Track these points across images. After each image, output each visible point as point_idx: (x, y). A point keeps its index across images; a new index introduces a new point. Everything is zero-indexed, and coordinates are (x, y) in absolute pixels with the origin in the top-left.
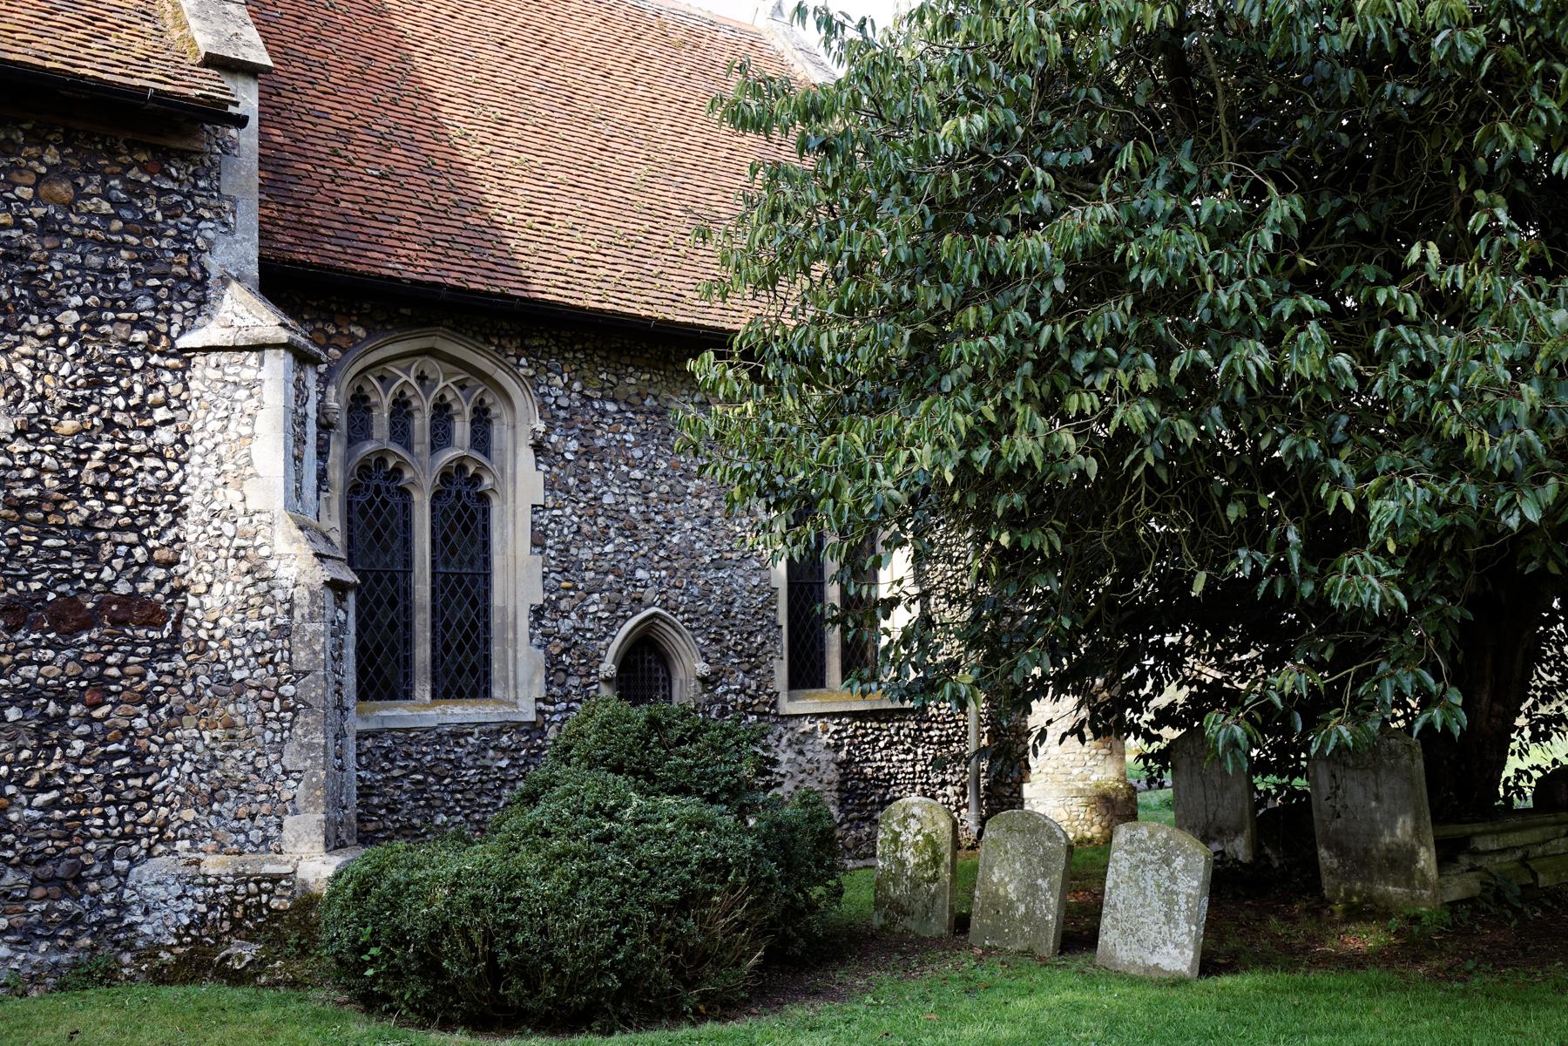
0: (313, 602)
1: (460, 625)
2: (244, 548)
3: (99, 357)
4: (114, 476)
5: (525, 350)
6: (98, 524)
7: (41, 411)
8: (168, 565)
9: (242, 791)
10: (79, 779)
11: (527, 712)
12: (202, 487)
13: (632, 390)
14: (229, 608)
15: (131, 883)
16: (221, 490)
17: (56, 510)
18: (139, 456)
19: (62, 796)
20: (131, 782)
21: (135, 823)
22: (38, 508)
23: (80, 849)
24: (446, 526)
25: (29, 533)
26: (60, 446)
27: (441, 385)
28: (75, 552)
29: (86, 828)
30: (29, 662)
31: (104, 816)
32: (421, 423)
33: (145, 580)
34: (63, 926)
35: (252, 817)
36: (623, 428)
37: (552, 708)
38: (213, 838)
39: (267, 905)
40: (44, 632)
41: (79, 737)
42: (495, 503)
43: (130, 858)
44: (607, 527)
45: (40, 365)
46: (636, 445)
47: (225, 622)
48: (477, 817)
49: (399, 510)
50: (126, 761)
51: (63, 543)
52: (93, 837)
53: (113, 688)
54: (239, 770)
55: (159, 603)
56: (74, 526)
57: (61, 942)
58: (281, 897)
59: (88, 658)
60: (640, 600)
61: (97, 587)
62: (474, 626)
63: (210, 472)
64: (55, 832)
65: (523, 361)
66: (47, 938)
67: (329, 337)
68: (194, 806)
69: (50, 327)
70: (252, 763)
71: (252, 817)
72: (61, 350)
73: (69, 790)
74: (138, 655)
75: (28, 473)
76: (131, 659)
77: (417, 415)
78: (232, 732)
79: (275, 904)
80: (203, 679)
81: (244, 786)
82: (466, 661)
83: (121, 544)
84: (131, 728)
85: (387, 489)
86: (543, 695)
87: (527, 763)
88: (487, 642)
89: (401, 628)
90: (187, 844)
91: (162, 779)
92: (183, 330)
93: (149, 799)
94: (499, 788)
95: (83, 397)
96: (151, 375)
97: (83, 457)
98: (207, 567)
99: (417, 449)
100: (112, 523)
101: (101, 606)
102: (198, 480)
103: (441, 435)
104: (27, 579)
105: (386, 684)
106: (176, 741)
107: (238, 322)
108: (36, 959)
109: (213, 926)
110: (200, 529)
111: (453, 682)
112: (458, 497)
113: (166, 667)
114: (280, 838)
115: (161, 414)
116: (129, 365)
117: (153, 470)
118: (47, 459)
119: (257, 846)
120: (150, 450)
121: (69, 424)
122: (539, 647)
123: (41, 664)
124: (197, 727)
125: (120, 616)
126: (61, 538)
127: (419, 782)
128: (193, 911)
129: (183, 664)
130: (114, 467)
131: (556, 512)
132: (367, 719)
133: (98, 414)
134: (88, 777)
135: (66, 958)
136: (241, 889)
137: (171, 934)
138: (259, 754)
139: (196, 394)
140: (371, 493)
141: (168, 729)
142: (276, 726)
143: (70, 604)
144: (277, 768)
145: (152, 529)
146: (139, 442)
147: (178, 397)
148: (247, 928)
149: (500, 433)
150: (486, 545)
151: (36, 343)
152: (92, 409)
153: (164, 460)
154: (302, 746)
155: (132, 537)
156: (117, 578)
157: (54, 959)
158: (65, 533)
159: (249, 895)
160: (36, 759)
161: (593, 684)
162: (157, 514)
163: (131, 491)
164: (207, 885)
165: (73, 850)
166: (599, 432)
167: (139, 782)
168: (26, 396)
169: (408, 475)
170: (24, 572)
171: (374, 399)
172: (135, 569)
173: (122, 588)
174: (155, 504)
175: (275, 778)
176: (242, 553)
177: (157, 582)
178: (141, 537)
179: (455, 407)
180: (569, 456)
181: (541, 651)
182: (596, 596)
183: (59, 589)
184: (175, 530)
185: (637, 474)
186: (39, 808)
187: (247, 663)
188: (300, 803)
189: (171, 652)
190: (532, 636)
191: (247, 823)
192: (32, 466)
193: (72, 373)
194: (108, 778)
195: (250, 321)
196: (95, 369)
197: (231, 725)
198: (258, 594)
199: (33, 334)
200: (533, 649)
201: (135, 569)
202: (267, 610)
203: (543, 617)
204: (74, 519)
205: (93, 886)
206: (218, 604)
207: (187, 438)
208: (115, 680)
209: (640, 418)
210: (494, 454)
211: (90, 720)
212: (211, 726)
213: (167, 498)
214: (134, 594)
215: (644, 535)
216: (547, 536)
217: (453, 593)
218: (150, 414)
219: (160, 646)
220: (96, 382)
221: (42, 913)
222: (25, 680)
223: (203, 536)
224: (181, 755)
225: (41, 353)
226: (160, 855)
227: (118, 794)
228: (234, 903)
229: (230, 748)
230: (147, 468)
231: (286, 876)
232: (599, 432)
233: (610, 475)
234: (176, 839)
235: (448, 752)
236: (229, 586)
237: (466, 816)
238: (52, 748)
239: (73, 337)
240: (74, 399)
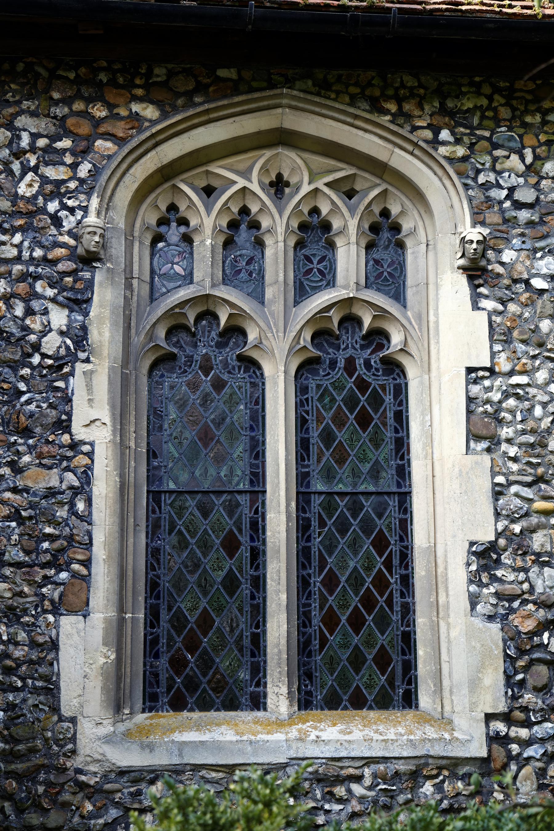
1: (356, 580)
5: (454, 118)
11: (472, 742)
24: (328, 416)
27: (306, 189)
37: (524, 733)
62: (381, 583)
65: (445, 135)
67: (97, 122)
82: (369, 643)
86: (502, 707)
88: (408, 611)
89: (245, 589)
105: (219, 686)
122: (491, 618)
131: (516, 379)
132: (151, 748)
150: (402, 446)
180: (538, 283)
200: (478, 623)
216: (500, 422)
217: (343, 527)
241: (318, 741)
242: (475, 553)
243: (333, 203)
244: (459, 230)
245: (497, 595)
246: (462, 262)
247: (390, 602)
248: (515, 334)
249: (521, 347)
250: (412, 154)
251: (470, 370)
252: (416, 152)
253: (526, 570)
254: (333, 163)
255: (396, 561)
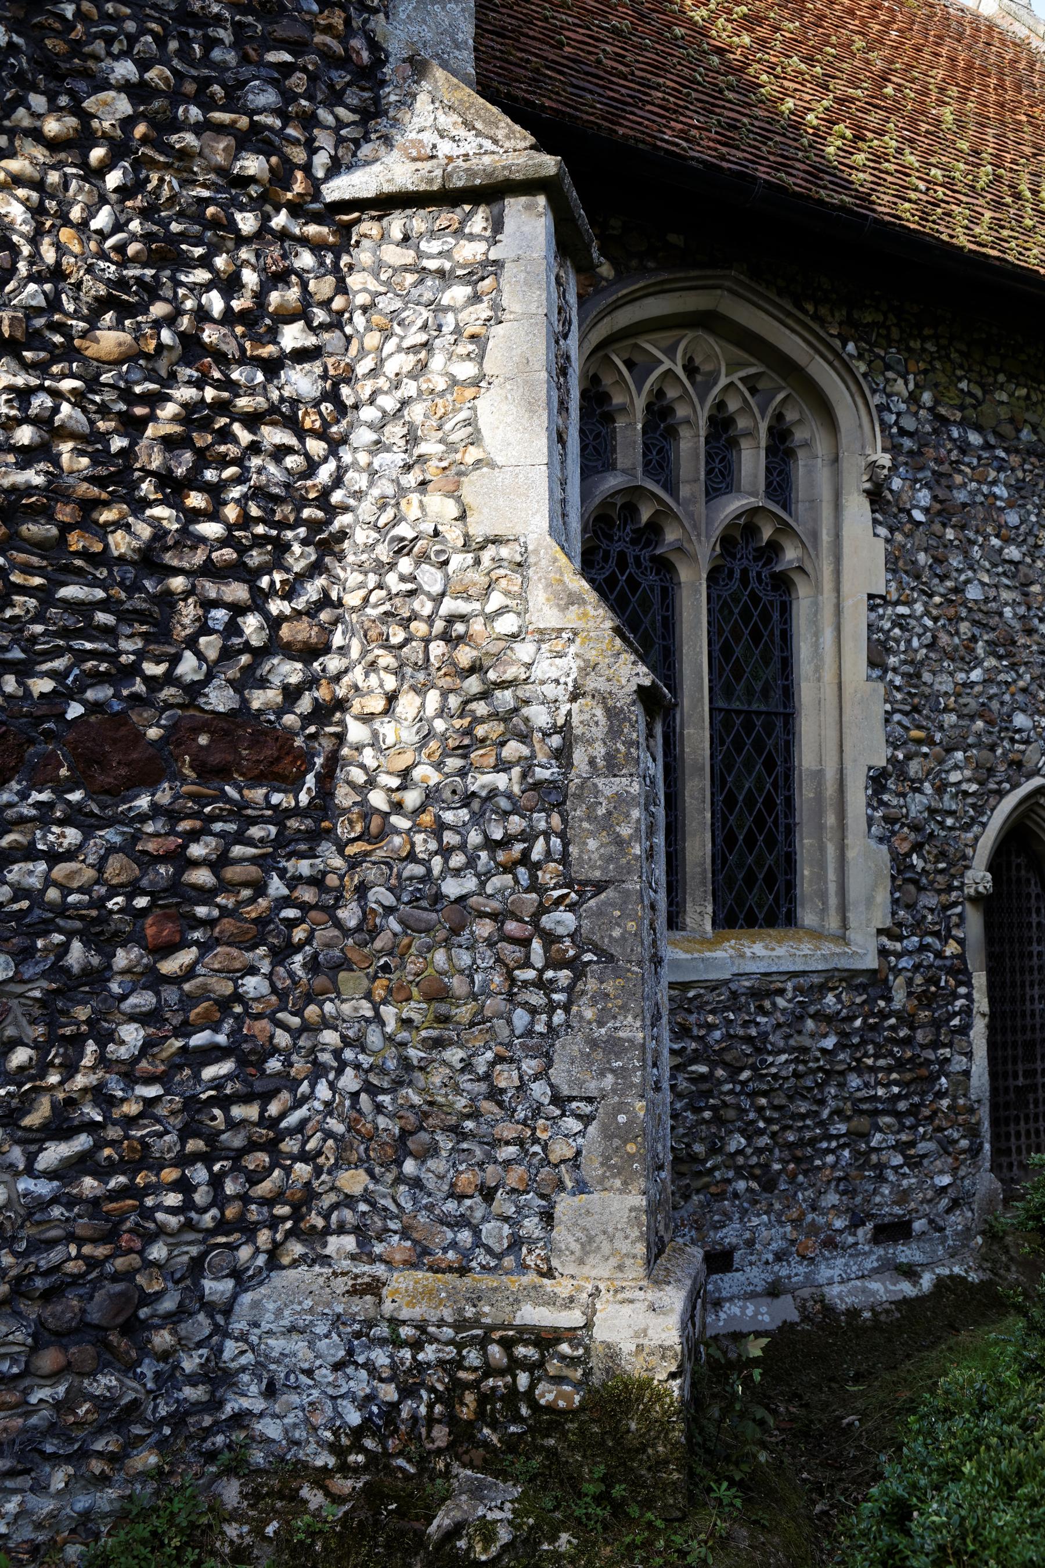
0: (613, 733)
2: (463, 618)
3: (173, 199)
4: (203, 460)
5: (853, 329)
6: (170, 559)
7: (54, 304)
8: (310, 653)
9: (463, 1136)
10: (132, 1109)
12: (376, 492)
13: (1003, 413)
14: (433, 745)
15: (238, 1326)
16: (415, 497)
17: (86, 522)
18: (253, 421)
19: (98, 1146)
20: (237, 1112)
21: (245, 1199)
22: (45, 513)
23: (135, 1260)
25: (28, 570)
26: (93, 384)
27: (723, 381)
28: (125, 616)
29: (147, 1214)
30: (29, 853)
31: (184, 1186)
32: (690, 446)
33: (263, 683)
34: (100, 1430)
35: (488, 1194)
36: (993, 474)
37: (898, 946)
38: (405, 1233)
39: (529, 1395)
40: (61, 788)
41: (132, 1018)
42: (803, 590)
43: (237, 1274)
44: (974, 639)
45: (51, 205)
46: (1011, 505)
47: (426, 773)
48: (791, 1137)
49: (656, 598)
50: (226, 1067)
51: (100, 594)
52: (162, 1230)
53: (201, 911)
54: (458, 1091)
55: (291, 733)
56: (121, 558)
57: (97, 1466)
58: (558, 1380)
59: (151, 846)
60: (1019, 764)
61: (168, 693)
62: (770, 803)
63: (391, 460)
64: (83, 1226)
66: (68, 1459)
68: (363, 1162)
69: (72, 121)
70: (487, 1077)
71: (488, 1194)
72: (95, 174)
73: (113, 1133)
74: (250, 842)
75: (25, 435)
76: (238, 850)
77: (684, 432)
78: (443, 1008)
79: (546, 1394)
80: (380, 895)
81: (469, 1125)
82: (760, 861)
83: (216, 604)
84: (237, 997)
85: (637, 558)
86: (888, 923)
87: (864, 1042)
88: (790, 831)
90: (349, 1242)
91: (298, 1104)
92: (335, 168)
93: (271, 1147)
94: (820, 1086)
95: (139, 280)
96: (275, 251)
97: (139, 411)
98: (387, 659)
99: (685, 491)
100: (199, 558)
101: (177, 735)
102: (367, 474)
103: (721, 478)
104: (24, 671)
106: (326, 1023)
107: (445, 148)
108: (46, 1506)
109: (413, 1435)
110: (372, 580)
111: (740, 901)
112: (745, 580)
113: (304, 867)
114: (548, 1243)
115: (293, 336)
116: (232, 226)
117: (280, 453)
118: (66, 408)
119: (499, 1256)
120: (273, 409)
121: (109, 339)
122: (881, 840)
123: (53, 857)
124: (368, 996)
125: (215, 759)
126: (95, 583)
127: (703, 1077)
128: (370, 1398)
129: (338, 862)
130: (203, 439)
133: (170, 321)
134: (150, 1102)
135: (107, 1498)
136: (473, 1357)
137: (321, 1443)
138: (499, 1059)
139: (361, 299)
140: (612, 563)
141: (310, 998)
142: (536, 999)
143: (112, 726)
144: (539, 1090)
145: (278, 577)
146: (252, 391)
147: (326, 304)
148: (486, 1444)
149: (811, 473)
150: (787, 665)
151: (40, 153)
152: (159, 309)
153: (301, 434)
154: (593, 1043)
155: (237, 591)
156: (210, 676)
157: (82, 1503)
158: (102, 573)
159: (489, 1370)
160: (43, 1068)
161: (955, 904)
162: (287, 547)
163: (236, 492)
164: (398, 1343)
165: (120, 1263)
166: (958, 479)
167: (252, 1112)
168: (22, 267)
169: (671, 535)
170: (17, 654)
171: (618, 400)
172: (245, 659)
173: (219, 699)
174: (283, 525)
175: (537, 1111)
176: (459, 628)
177: (286, 688)
178: (256, 591)
179: (742, 423)
180: (918, 516)
181: (884, 848)
182: (959, 755)
183: (90, 695)
184: (321, 581)
185: (1013, 552)
186: (50, 1175)
187: (471, 862)
188: (592, 1169)
189: (315, 836)
190: (870, 821)
191: (474, 1204)
192: (35, 421)
193: (118, 227)
194: (191, 1104)
195: (470, 145)
196: (165, 224)
197: (438, 994)
198: (494, 716)
199: (37, 135)
200: (873, 843)
201: (245, 659)
202: (513, 749)
203: (884, 789)
204: (120, 543)
205: (163, 1339)
206: (410, 736)
207: (345, 391)
208: (206, 895)
209: (1014, 460)
210: (801, 508)
211: (154, 980)
212: (397, 995)
213: (306, 513)
214: (242, 713)
215: (1024, 655)
218: (273, 335)
219: (293, 823)
220: (166, 254)
221: (58, 1406)
222: (20, 892)
223: (377, 595)
224: (337, 1053)
225: (53, 177)
226: (295, 1264)
227: (211, 1137)
228: (457, 1387)
229: (439, 1043)
230: (266, 445)
231: (569, 1334)
232: (958, 479)
233: (976, 552)
234: (327, 1231)
235: (746, 1024)
236: (433, 698)
237: (773, 1135)
238: (77, 1041)
239: (119, 150)
240: (122, 283)
241: (754, 957)
242: (871, 778)
243: (745, 400)
244: (869, 451)
245: (886, 819)
246: (868, 485)
247: (776, 823)
248: (901, 563)
249: (906, 578)
250: (830, 364)
251: (871, 597)
252: (836, 363)
253: (904, 795)
254: (752, 360)
255: (781, 783)
